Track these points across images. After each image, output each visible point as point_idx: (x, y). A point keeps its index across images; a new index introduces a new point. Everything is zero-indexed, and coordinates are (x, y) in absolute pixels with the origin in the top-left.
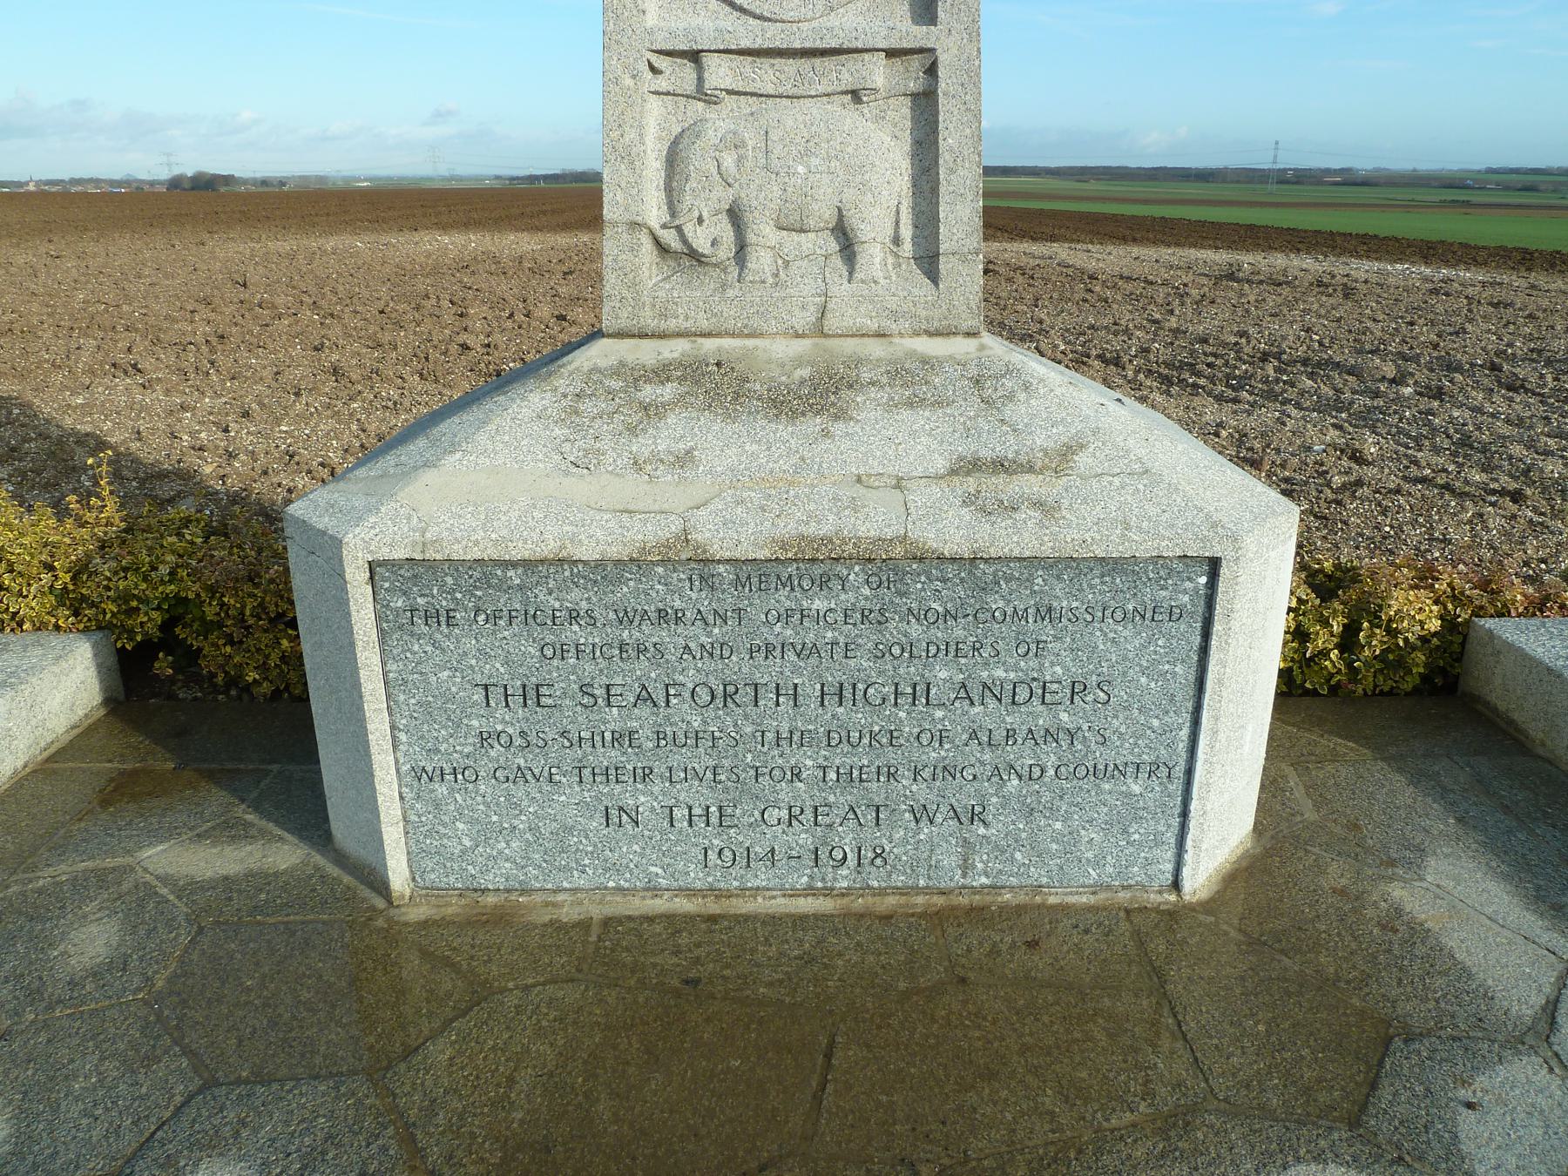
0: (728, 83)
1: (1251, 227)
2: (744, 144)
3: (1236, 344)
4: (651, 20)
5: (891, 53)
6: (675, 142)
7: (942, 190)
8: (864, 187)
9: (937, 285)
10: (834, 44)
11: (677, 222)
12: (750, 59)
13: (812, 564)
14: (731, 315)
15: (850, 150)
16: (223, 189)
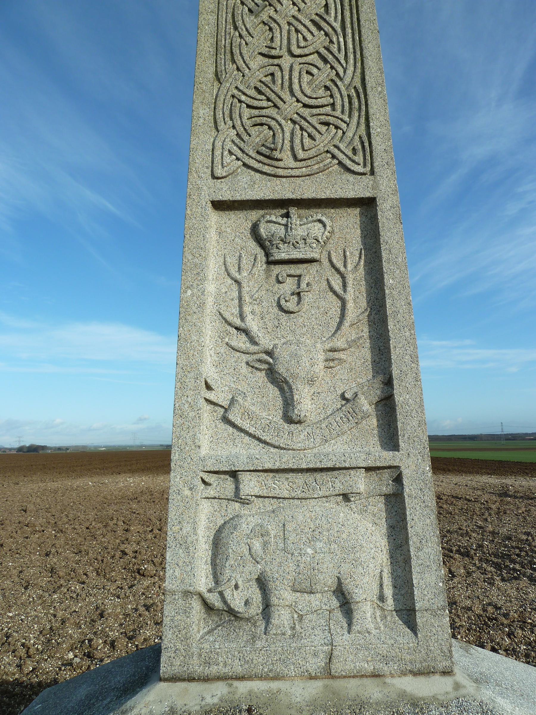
0: (257, 491)
1: (500, 462)
2: (268, 534)
3: (527, 540)
4: (204, 451)
5: (368, 469)
6: (219, 531)
7: (413, 563)
8: (356, 563)
9: (416, 634)
10: (330, 465)
11: (220, 589)
12: (271, 475)
14: (259, 662)
15: (344, 536)
16: (41, 452)
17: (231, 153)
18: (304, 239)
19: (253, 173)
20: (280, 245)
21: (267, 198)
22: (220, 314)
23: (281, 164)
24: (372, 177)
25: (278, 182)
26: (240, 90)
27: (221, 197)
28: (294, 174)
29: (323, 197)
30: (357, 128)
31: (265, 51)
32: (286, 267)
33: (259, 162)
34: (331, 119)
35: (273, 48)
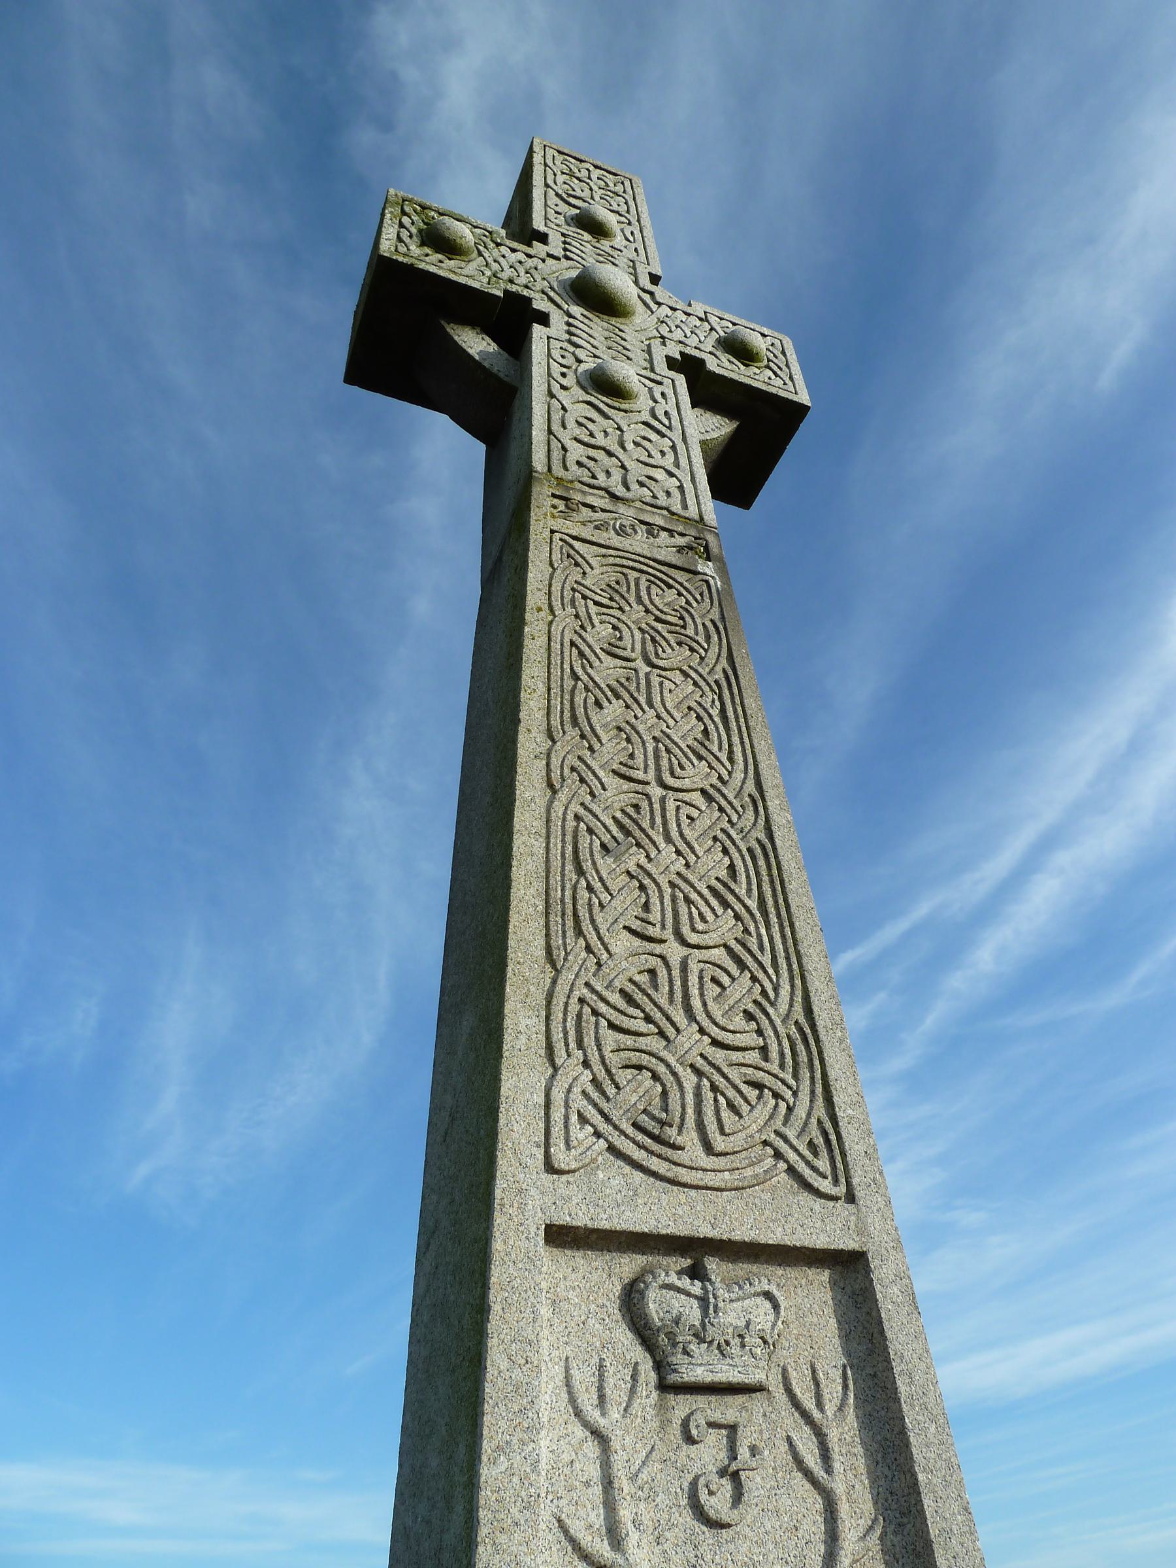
17: (583, 1120)
18: (740, 1336)
19: (627, 1169)
20: (692, 1346)
21: (664, 1232)
22: (559, 1521)
23: (676, 1155)
24: (850, 1207)
25: (682, 1197)
26: (593, 990)
27: (568, 1218)
28: (710, 1184)
29: (771, 1242)
30: (811, 1101)
31: (636, 925)
32: (701, 1401)
33: (639, 1146)
34: (768, 1080)
35: (650, 923)
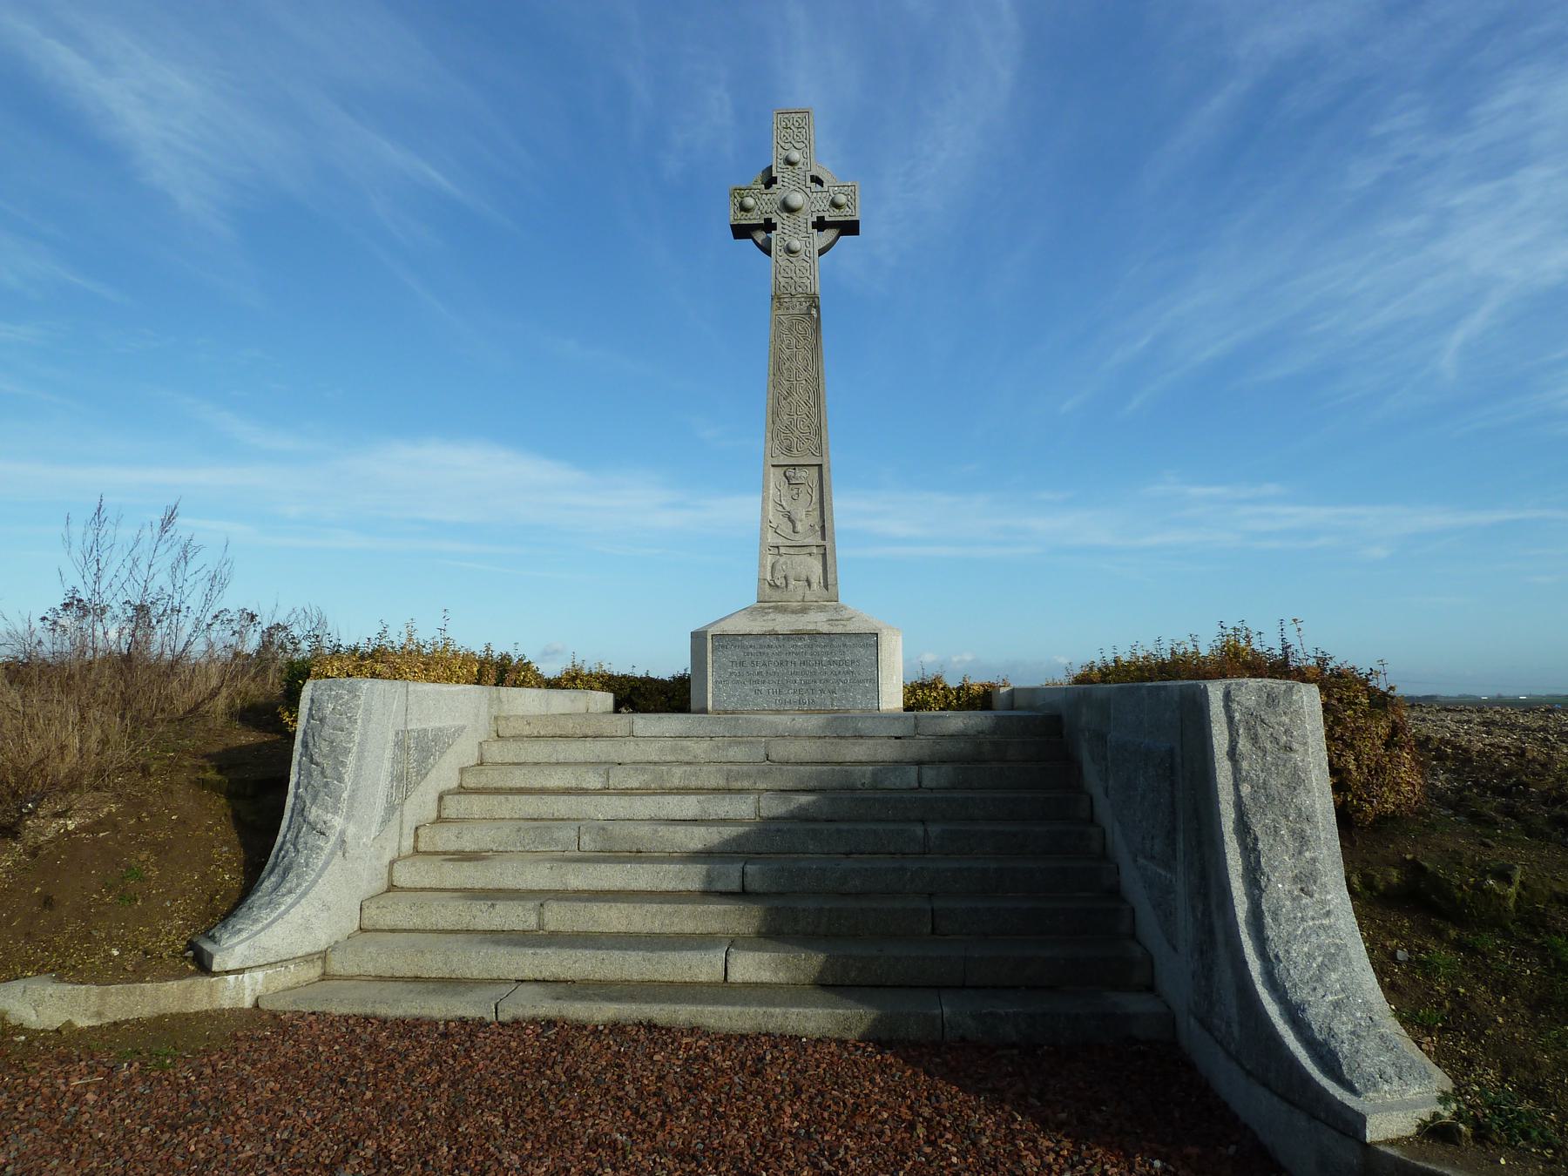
13: (799, 635)
